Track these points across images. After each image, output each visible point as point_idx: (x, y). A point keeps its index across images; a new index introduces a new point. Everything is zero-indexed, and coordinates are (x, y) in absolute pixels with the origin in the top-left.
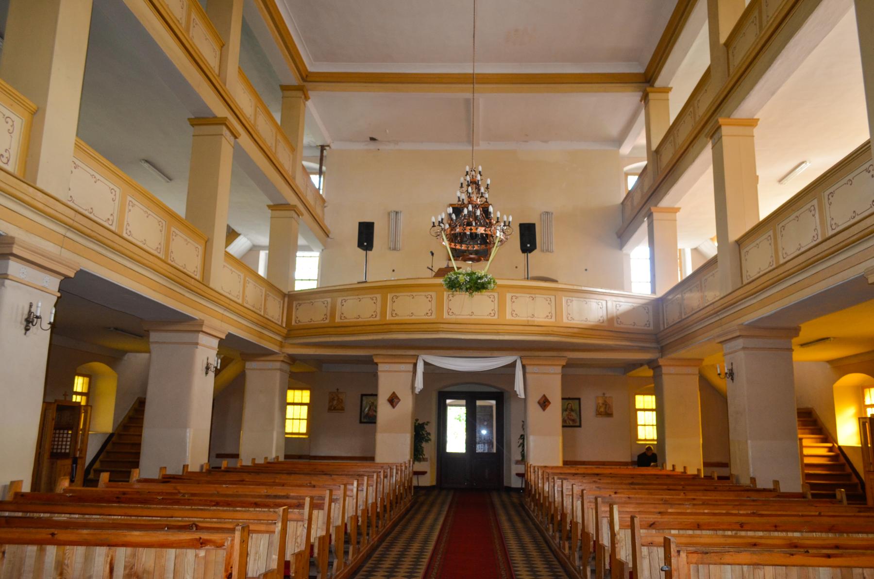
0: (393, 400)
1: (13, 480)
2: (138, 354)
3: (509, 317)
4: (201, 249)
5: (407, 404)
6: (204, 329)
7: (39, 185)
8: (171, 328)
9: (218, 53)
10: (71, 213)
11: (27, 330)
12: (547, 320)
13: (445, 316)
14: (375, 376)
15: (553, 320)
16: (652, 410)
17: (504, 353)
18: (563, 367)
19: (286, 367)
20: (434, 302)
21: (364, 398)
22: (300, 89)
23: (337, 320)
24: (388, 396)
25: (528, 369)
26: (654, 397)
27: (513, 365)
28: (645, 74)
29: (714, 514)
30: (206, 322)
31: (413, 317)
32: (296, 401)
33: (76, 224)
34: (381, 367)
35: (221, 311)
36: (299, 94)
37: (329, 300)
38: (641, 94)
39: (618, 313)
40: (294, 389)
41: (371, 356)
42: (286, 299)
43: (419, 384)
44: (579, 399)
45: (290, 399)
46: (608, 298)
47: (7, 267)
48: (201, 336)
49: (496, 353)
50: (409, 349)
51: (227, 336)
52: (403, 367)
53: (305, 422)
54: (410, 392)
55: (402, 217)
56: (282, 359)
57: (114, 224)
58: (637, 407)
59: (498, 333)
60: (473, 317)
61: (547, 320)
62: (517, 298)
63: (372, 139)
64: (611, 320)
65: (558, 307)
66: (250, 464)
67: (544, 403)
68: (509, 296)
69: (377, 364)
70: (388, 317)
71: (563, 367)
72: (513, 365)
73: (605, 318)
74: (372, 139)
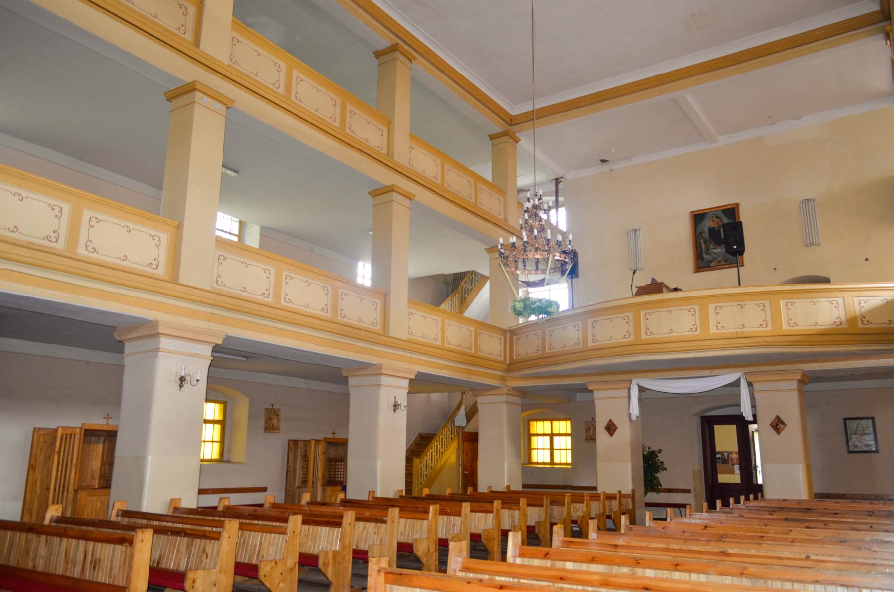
0: (611, 428)
1: (173, 497)
2: (417, 395)
3: (713, 330)
4: (379, 303)
5: (624, 432)
6: (384, 372)
7: (181, 281)
8: (361, 373)
9: (386, 131)
10: (213, 296)
11: (181, 386)
12: (761, 329)
13: (643, 336)
14: (591, 404)
15: (770, 328)
16: (566, 435)
17: (725, 370)
18: (799, 381)
19: (519, 400)
20: (631, 323)
21: (848, 421)
22: (505, 134)
23: (547, 350)
24: (605, 423)
25: (756, 386)
26: (569, 422)
27: (737, 384)
28: (882, 10)
29: (667, 550)
30: (384, 366)
31: (613, 341)
32: (562, 432)
33: (217, 303)
34: (597, 395)
35: (409, 355)
36: (506, 138)
37: (540, 332)
38: (881, 36)
39: (863, 310)
40: (559, 420)
41: (585, 384)
42: (508, 335)
43: (635, 410)
44: (873, 418)
45: (534, 430)
46: (845, 294)
47: (159, 343)
48: (383, 378)
49: (716, 372)
50: (620, 374)
51: (416, 376)
52: (618, 393)
53: (569, 452)
54: (627, 420)
55: (641, 235)
56: (506, 392)
57: (271, 295)
58: (532, 432)
59: (698, 350)
60: (673, 334)
61: (761, 329)
62: (721, 308)
63: (603, 161)
64: (852, 321)
65: (776, 313)
66: (486, 491)
67: (778, 425)
68: (711, 307)
69: (591, 391)
70: (590, 343)
71: (799, 381)
72: (737, 384)
73: (843, 318)
74: (603, 161)
